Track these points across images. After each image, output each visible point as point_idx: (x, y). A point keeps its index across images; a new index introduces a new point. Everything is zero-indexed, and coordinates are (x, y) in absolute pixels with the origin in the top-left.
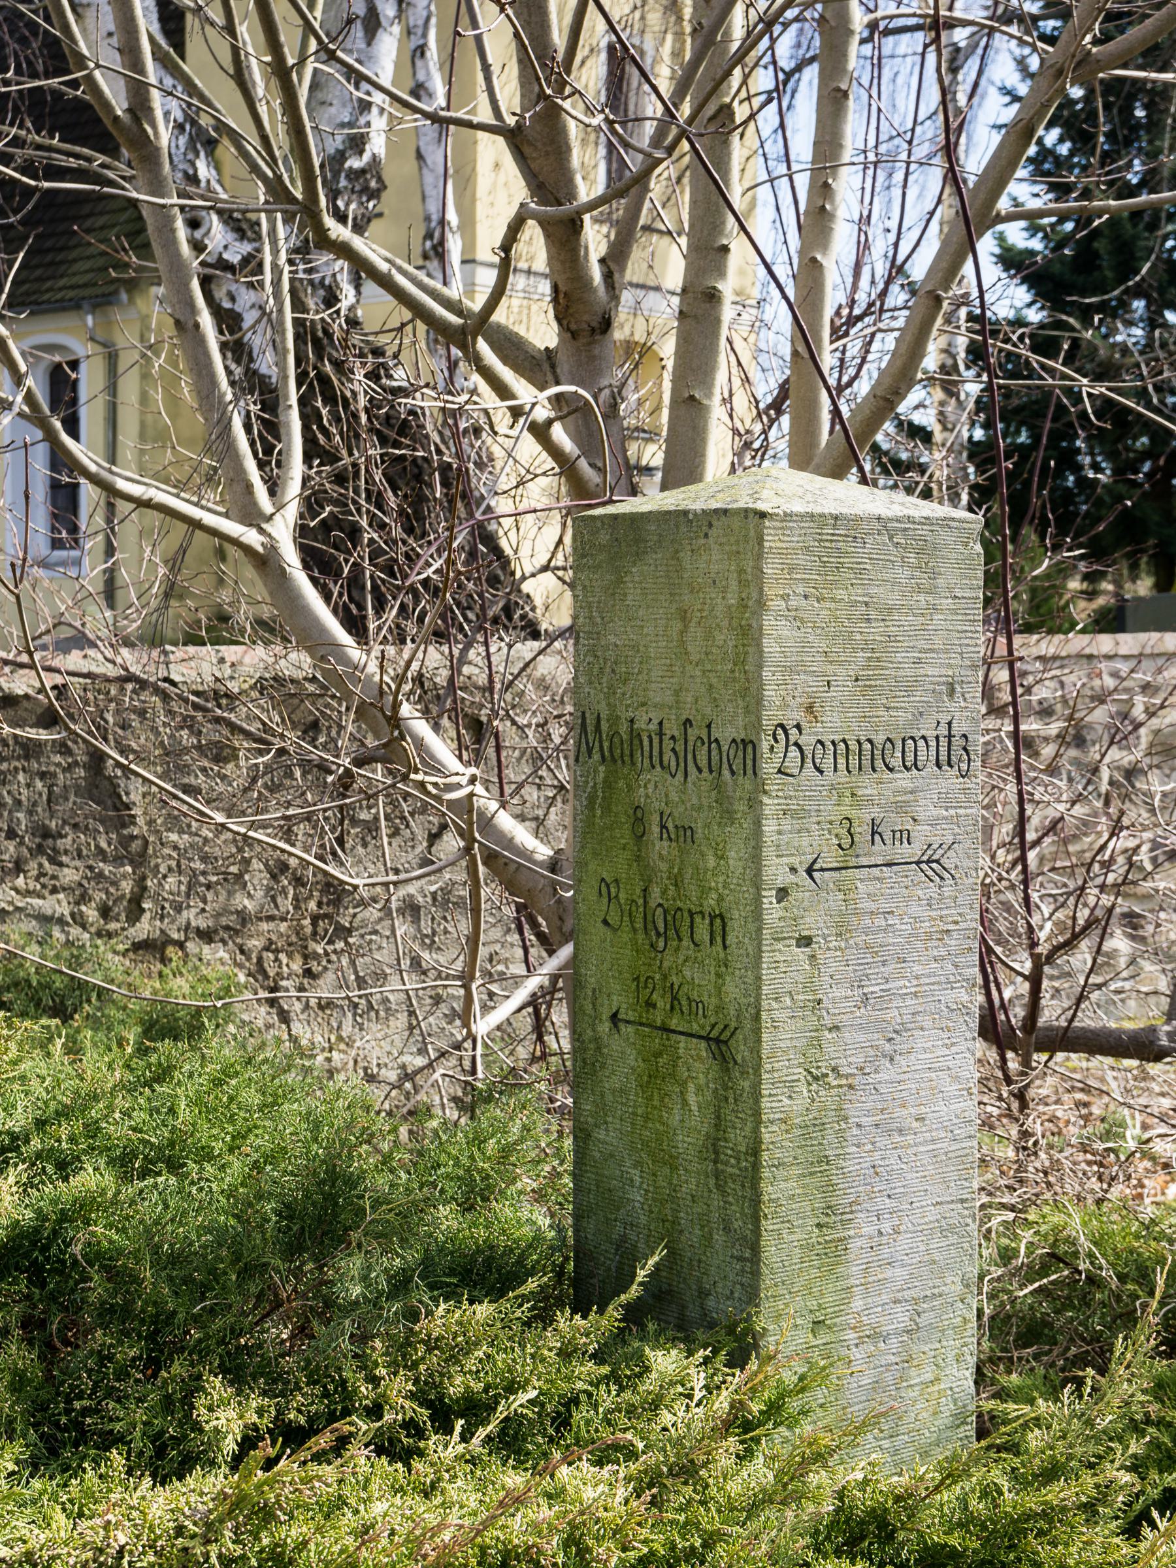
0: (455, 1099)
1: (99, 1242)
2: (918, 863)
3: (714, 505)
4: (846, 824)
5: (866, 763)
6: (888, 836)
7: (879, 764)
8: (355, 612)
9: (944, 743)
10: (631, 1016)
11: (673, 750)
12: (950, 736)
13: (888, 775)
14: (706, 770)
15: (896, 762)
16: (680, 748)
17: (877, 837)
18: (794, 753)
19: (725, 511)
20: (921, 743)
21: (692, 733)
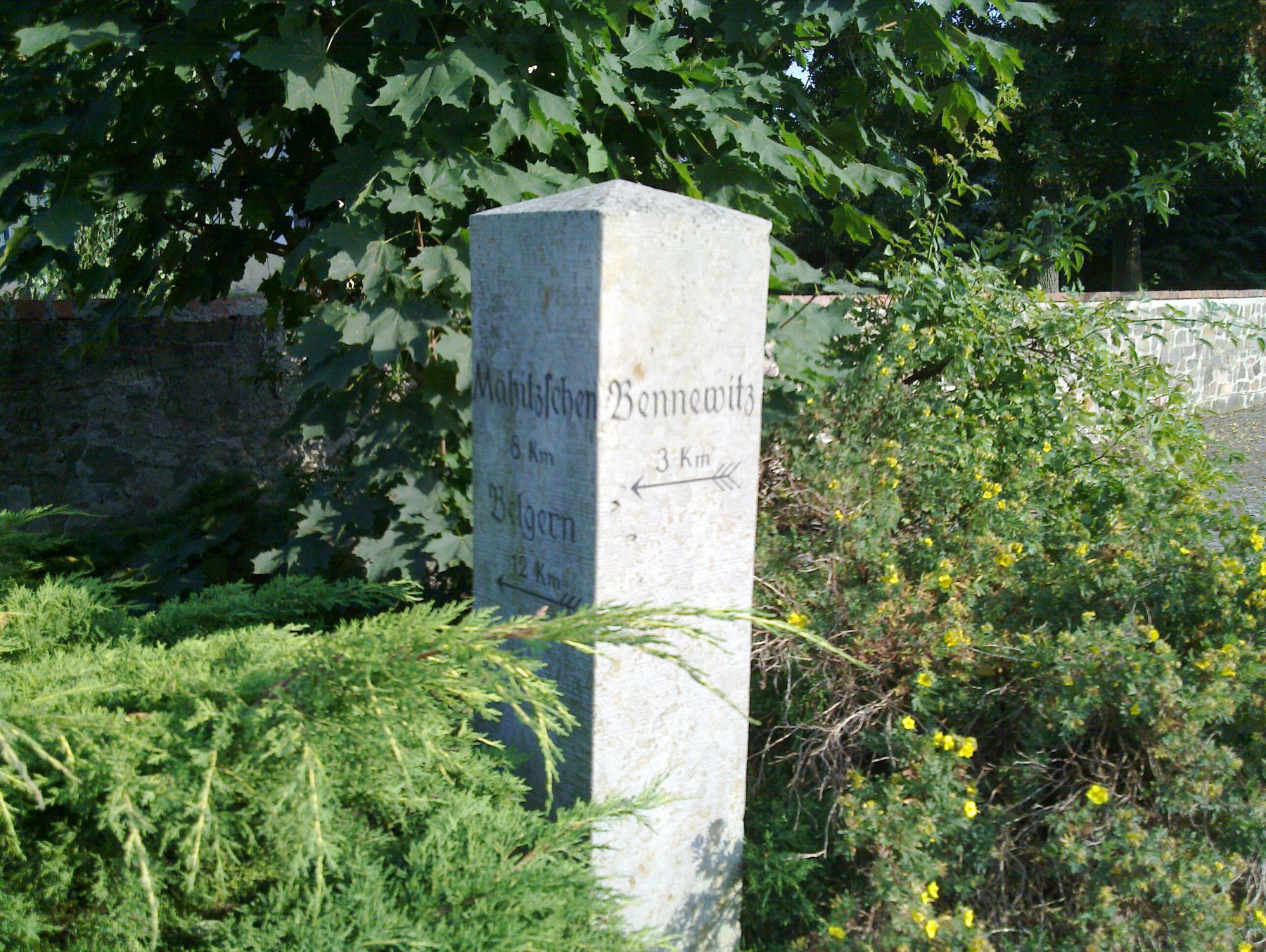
0: (521, 804)
1: (958, 459)
2: (714, 478)
3: (570, 208)
4: (663, 453)
5: (679, 407)
6: (693, 460)
7: (688, 407)
8: (239, 38)
9: (735, 392)
10: (511, 582)
11: (539, 396)
12: (740, 387)
13: (694, 416)
14: (561, 413)
15: (700, 406)
16: (543, 393)
17: (685, 462)
18: (624, 401)
19: (576, 213)
20: (719, 393)
21: (552, 384)
